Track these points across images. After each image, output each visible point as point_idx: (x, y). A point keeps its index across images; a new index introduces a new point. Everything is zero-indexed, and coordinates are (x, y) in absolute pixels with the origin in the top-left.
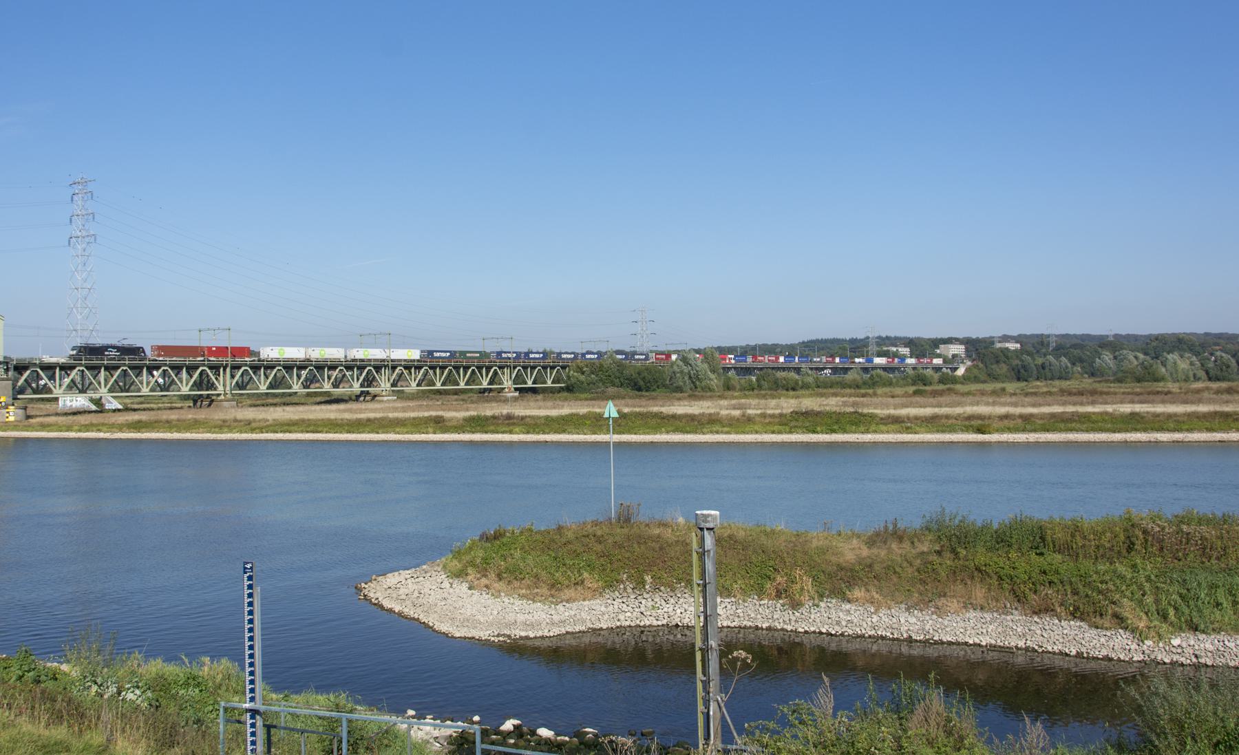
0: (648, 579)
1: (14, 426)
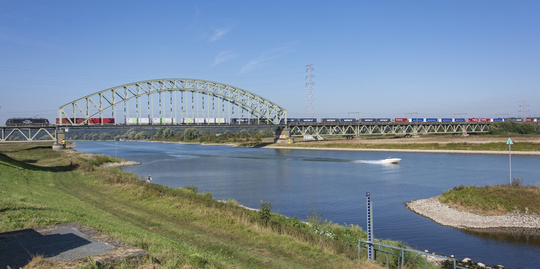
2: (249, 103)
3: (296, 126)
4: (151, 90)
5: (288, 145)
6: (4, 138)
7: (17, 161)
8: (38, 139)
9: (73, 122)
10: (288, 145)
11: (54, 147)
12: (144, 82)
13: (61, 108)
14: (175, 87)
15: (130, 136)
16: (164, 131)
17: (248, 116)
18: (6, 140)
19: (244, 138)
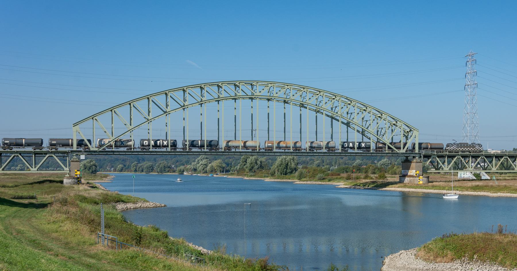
0: (475, 257)
1: (421, 187)
2: (357, 120)
3: (433, 155)
4: (204, 99)
5: (418, 186)
8: (10, 169)
10: (418, 186)
11: (65, 181)
12: (212, 84)
13: (75, 125)
16: (249, 161)
17: (355, 138)
19: (374, 173)
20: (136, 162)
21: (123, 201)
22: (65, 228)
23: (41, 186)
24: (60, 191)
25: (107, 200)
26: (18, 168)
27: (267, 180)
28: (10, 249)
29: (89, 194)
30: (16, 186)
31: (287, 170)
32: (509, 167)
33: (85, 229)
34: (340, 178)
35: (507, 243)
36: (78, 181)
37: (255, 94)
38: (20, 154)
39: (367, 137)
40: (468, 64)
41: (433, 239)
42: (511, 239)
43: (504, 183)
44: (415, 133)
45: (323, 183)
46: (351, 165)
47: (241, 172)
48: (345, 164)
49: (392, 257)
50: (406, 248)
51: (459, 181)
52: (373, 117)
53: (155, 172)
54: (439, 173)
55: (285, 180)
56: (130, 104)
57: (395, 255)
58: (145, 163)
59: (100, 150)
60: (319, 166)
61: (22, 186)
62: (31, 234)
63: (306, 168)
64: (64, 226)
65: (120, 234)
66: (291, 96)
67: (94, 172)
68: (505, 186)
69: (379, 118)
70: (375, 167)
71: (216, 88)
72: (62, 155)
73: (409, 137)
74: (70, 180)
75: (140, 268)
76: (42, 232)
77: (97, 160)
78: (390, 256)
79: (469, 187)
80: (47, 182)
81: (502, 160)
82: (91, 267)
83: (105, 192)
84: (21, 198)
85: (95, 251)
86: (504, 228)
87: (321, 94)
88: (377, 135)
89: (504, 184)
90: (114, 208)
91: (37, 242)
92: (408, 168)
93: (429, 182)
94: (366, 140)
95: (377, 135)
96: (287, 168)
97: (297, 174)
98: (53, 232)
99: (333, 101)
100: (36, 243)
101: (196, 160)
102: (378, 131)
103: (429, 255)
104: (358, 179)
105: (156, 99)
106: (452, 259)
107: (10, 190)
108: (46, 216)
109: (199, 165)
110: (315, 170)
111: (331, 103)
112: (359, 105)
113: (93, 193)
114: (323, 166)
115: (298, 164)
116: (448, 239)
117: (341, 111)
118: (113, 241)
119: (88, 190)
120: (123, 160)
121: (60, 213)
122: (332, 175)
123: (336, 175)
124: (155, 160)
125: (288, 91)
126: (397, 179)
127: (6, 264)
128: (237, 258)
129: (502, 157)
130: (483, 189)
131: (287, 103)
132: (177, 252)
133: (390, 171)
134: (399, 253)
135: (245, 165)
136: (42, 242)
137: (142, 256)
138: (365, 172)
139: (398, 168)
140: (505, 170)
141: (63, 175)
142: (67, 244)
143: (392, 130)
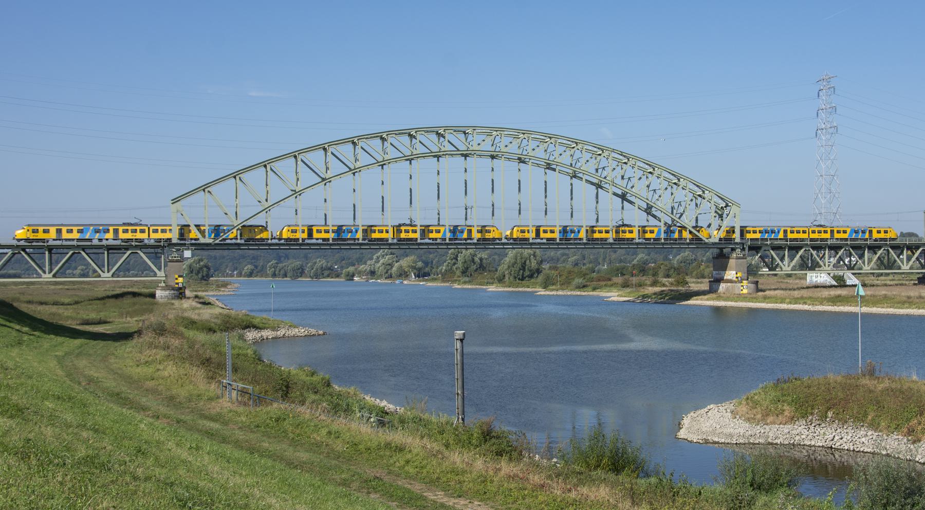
0: (830, 414)
2: (639, 188)
6: (45, 272)
7: (42, 322)
9: (204, 237)
11: (159, 293)
13: (175, 201)
14: (449, 147)
15: (379, 267)
18: (54, 276)
19: (668, 276)
20: (274, 262)
21: (256, 327)
22: (166, 374)
23: (118, 302)
24: (151, 311)
25: (229, 325)
26: (78, 272)
27: (492, 288)
28: (91, 410)
29: (199, 315)
30: (77, 303)
31: (525, 273)
32: (891, 265)
33: (199, 374)
34: (612, 285)
35: (882, 392)
36: (180, 293)
37: (471, 148)
38: (83, 250)
39: (655, 216)
40: (821, 94)
41: (761, 386)
42: (888, 385)
43: (883, 292)
44: (734, 210)
45: (584, 294)
46: (630, 262)
47: (447, 276)
48: (621, 261)
49: (695, 415)
50: (720, 399)
51: (808, 288)
52: (665, 184)
53: (306, 277)
54: (776, 275)
55: (520, 289)
56: (265, 166)
57: (698, 412)
58: (290, 261)
59: (217, 242)
60: (577, 264)
61: (86, 303)
62: (110, 383)
63: (556, 268)
64: (164, 369)
65: (254, 382)
66: (530, 150)
67: (206, 278)
68: (885, 296)
69: (675, 186)
70: (669, 266)
71: (379, 141)
72: (152, 250)
73: (725, 216)
74: (167, 292)
75: (291, 435)
76: (130, 380)
77: (209, 257)
78: (692, 414)
79: (825, 298)
80: (129, 296)
81: (880, 252)
82: (212, 435)
83: (225, 312)
84: (87, 323)
85: (218, 410)
86: (877, 369)
87: (580, 146)
88: (672, 213)
89: (884, 292)
90: (242, 338)
91: (123, 395)
92: (724, 268)
93: (758, 290)
94: (653, 221)
95: (672, 213)
96: (524, 269)
97: (541, 278)
98: (147, 380)
99: (599, 158)
100: (121, 398)
101: (375, 257)
102: (673, 208)
103: (755, 411)
104: (641, 286)
105: (309, 157)
106: (792, 418)
107: (67, 309)
108: (131, 352)
109: (379, 264)
110: (570, 272)
111: (595, 162)
112: (642, 165)
113: (206, 314)
114: (584, 264)
115: (541, 262)
116: (785, 386)
117: (612, 173)
118: (243, 392)
119: (200, 308)
120: (254, 258)
121: (156, 347)
122: (599, 280)
123: (605, 281)
124: (306, 257)
125: (525, 142)
126: (705, 286)
127: (90, 432)
128: (443, 419)
129: (879, 247)
130: (848, 302)
131: (524, 162)
132: (348, 410)
133: (695, 273)
134: (706, 410)
135: (454, 264)
136: (131, 396)
137: (293, 417)
138: (654, 275)
139: (708, 267)
140: (886, 269)
141: (155, 285)
142: (171, 398)
143: (696, 205)
